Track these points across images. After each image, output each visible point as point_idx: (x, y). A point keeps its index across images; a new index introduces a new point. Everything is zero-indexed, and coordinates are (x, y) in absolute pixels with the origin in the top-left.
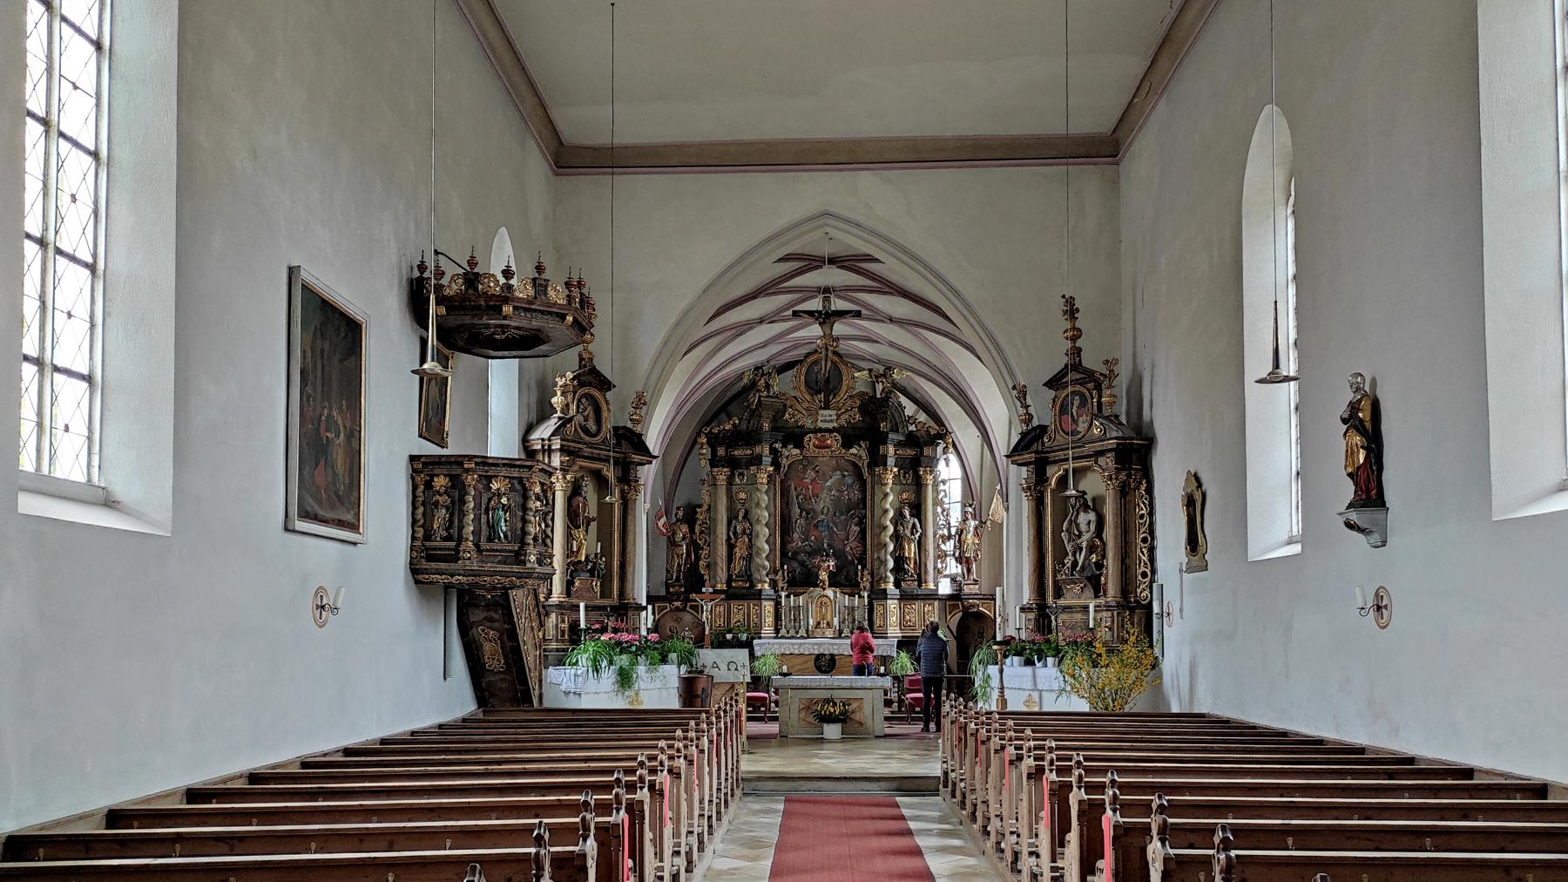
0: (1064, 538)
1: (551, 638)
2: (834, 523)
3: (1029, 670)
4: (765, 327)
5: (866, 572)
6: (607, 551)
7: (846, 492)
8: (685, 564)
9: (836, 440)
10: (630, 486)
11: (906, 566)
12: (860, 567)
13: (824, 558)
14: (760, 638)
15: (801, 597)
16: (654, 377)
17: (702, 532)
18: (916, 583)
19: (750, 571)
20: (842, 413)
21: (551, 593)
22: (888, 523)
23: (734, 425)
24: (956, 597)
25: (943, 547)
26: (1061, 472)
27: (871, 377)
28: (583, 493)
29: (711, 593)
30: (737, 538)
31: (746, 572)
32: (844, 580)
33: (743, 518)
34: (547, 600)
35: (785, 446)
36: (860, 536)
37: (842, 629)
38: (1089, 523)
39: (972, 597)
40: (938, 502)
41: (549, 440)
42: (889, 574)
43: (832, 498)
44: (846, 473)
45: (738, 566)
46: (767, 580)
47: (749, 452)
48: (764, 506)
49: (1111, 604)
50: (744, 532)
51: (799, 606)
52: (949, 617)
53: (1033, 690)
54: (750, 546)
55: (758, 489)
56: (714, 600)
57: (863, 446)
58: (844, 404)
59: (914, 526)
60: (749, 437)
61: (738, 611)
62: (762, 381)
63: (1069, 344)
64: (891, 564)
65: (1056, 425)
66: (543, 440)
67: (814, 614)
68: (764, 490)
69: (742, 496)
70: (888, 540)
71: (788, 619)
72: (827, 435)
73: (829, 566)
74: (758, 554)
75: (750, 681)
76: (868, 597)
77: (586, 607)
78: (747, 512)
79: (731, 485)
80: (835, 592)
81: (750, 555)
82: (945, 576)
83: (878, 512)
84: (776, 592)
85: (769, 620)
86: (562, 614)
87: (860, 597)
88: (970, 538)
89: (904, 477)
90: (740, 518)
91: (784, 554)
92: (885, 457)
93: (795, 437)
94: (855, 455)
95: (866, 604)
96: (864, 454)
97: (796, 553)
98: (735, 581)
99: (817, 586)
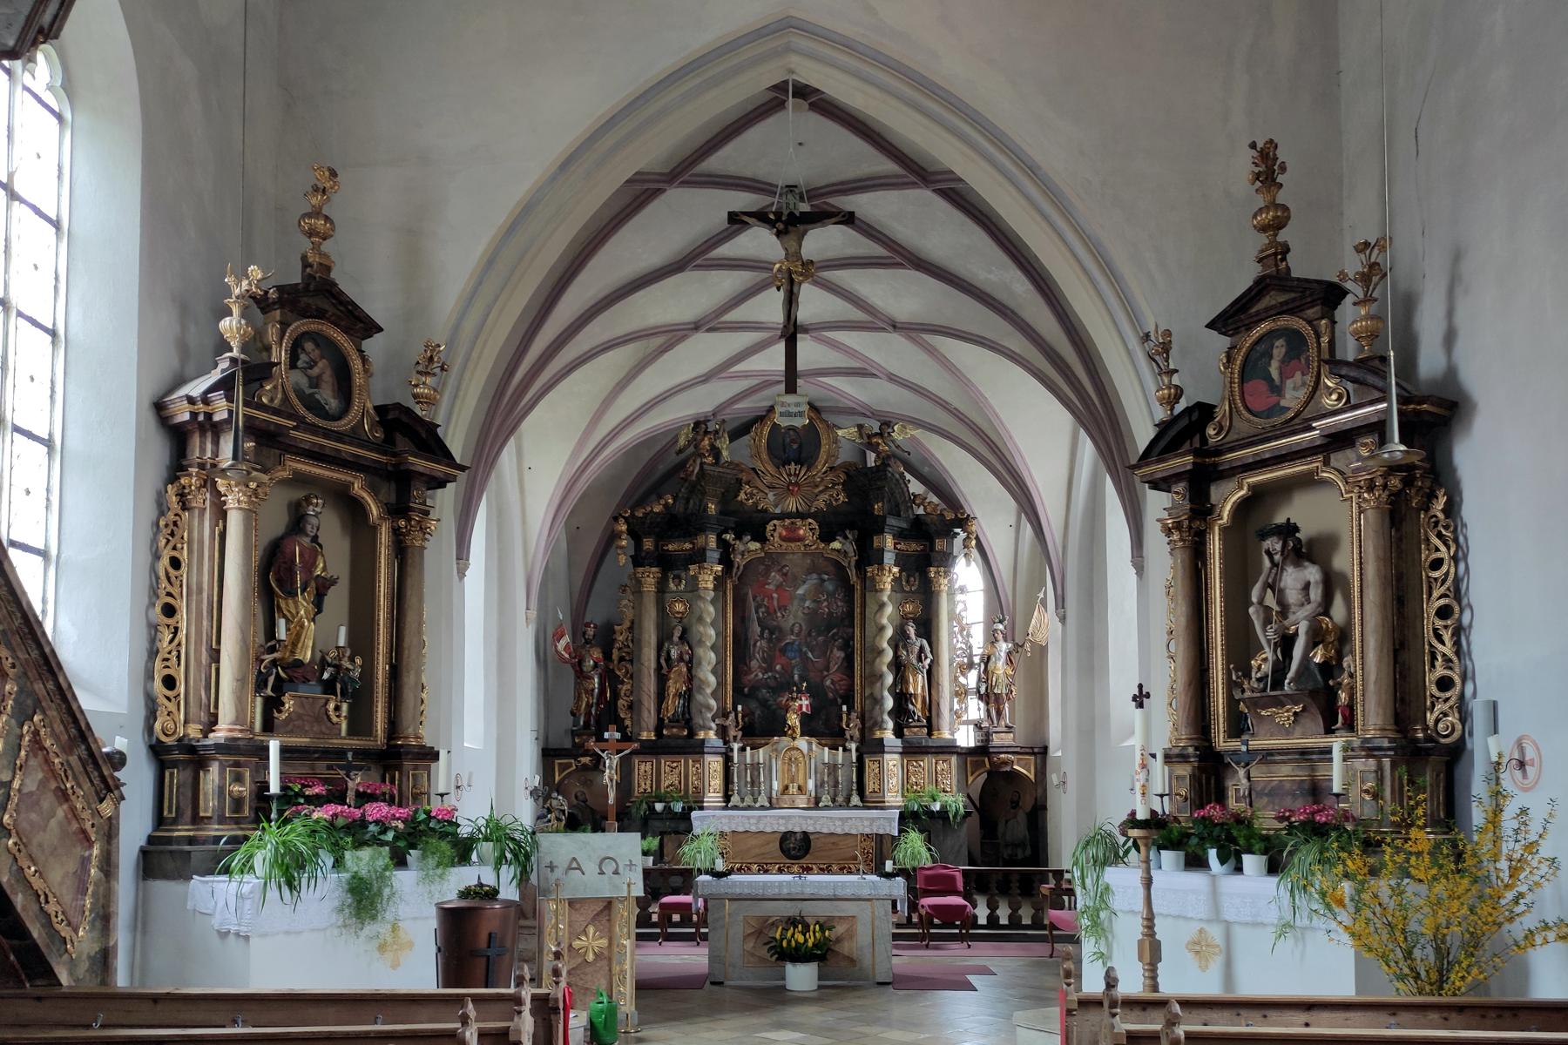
0: (1254, 617)
1: (209, 815)
2: (808, 647)
3: (1196, 879)
4: (701, 340)
5: (854, 715)
6: (361, 640)
7: (825, 604)
8: (598, 704)
9: (811, 529)
10: (409, 520)
11: (911, 706)
12: (844, 708)
13: (795, 695)
14: (701, 808)
15: (761, 750)
16: (469, 325)
17: (621, 659)
18: (925, 730)
19: (689, 714)
20: (821, 492)
21: (216, 723)
22: (885, 645)
23: (666, 505)
24: (982, 750)
25: (962, 680)
26: (1242, 493)
27: (861, 436)
28: (309, 528)
29: (617, 740)
30: (670, 667)
31: (683, 714)
32: (823, 727)
33: (680, 638)
34: (206, 737)
35: (739, 537)
36: (845, 664)
37: (819, 795)
38: (1307, 586)
39: (1005, 750)
40: (954, 617)
41: (206, 401)
42: (886, 717)
43: (806, 611)
44: (826, 577)
45: (673, 705)
46: (713, 725)
47: (688, 546)
48: (709, 620)
49: (1377, 743)
50: (681, 659)
51: (759, 763)
52: (970, 779)
53: (1209, 921)
54: (690, 678)
55: (700, 598)
56: (621, 751)
57: (850, 536)
58: (822, 479)
59: (922, 649)
60: (683, 524)
61: (671, 772)
62: (706, 442)
63: (1263, 239)
64: (889, 703)
65: (1232, 402)
66: (191, 400)
67: (780, 774)
68: (709, 599)
69: (679, 607)
70: (885, 669)
71: (743, 783)
72: (799, 522)
73: (801, 706)
74: (701, 690)
75: (642, 894)
76: (857, 750)
77: (285, 751)
78: (685, 631)
79: (664, 592)
80: (810, 744)
81: (689, 691)
82: (967, 723)
83: (870, 630)
84: (726, 742)
85: (717, 782)
86: (237, 764)
87: (845, 750)
88: (1000, 667)
89: (908, 582)
90: (676, 639)
91: (737, 690)
92: (881, 551)
93: (755, 525)
94: (838, 551)
95: (854, 760)
96: (850, 548)
97: (755, 688)
98: (668, 728)
99: (785, 734)
